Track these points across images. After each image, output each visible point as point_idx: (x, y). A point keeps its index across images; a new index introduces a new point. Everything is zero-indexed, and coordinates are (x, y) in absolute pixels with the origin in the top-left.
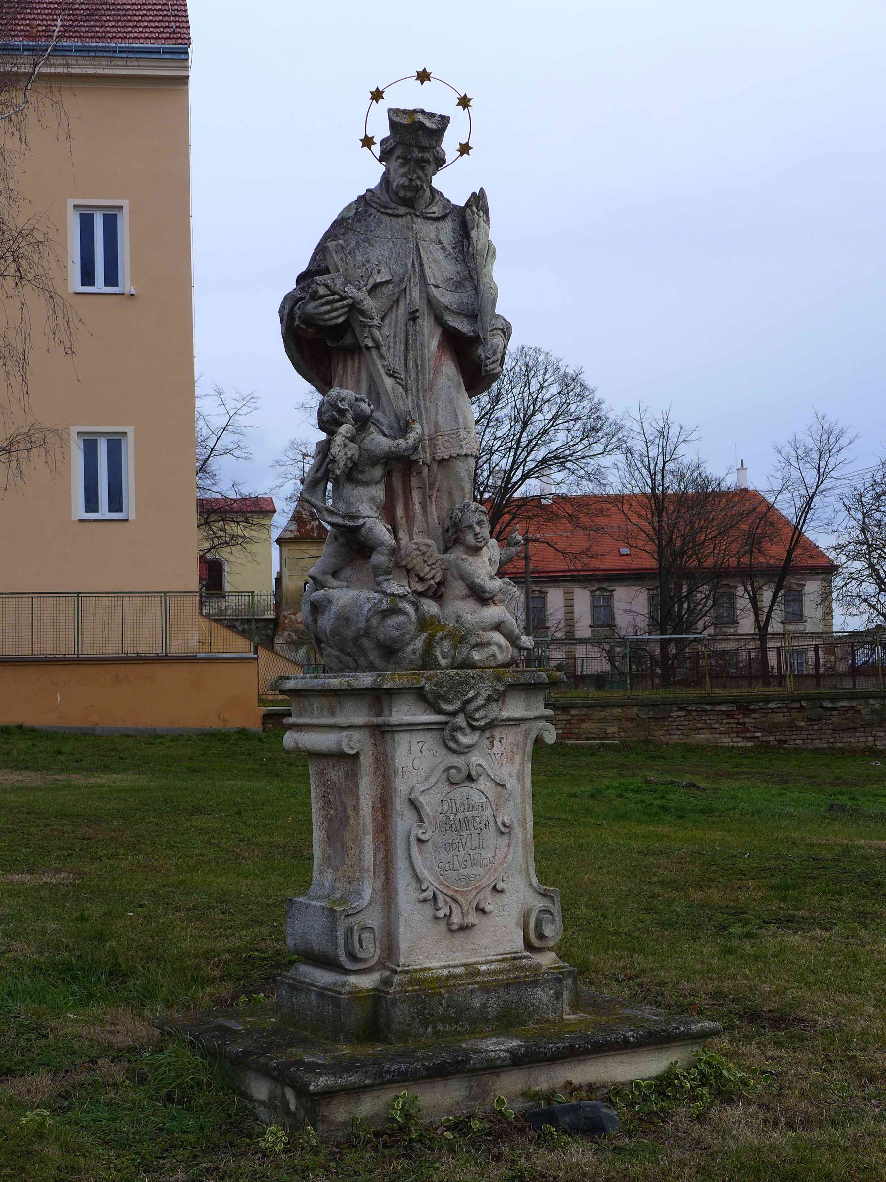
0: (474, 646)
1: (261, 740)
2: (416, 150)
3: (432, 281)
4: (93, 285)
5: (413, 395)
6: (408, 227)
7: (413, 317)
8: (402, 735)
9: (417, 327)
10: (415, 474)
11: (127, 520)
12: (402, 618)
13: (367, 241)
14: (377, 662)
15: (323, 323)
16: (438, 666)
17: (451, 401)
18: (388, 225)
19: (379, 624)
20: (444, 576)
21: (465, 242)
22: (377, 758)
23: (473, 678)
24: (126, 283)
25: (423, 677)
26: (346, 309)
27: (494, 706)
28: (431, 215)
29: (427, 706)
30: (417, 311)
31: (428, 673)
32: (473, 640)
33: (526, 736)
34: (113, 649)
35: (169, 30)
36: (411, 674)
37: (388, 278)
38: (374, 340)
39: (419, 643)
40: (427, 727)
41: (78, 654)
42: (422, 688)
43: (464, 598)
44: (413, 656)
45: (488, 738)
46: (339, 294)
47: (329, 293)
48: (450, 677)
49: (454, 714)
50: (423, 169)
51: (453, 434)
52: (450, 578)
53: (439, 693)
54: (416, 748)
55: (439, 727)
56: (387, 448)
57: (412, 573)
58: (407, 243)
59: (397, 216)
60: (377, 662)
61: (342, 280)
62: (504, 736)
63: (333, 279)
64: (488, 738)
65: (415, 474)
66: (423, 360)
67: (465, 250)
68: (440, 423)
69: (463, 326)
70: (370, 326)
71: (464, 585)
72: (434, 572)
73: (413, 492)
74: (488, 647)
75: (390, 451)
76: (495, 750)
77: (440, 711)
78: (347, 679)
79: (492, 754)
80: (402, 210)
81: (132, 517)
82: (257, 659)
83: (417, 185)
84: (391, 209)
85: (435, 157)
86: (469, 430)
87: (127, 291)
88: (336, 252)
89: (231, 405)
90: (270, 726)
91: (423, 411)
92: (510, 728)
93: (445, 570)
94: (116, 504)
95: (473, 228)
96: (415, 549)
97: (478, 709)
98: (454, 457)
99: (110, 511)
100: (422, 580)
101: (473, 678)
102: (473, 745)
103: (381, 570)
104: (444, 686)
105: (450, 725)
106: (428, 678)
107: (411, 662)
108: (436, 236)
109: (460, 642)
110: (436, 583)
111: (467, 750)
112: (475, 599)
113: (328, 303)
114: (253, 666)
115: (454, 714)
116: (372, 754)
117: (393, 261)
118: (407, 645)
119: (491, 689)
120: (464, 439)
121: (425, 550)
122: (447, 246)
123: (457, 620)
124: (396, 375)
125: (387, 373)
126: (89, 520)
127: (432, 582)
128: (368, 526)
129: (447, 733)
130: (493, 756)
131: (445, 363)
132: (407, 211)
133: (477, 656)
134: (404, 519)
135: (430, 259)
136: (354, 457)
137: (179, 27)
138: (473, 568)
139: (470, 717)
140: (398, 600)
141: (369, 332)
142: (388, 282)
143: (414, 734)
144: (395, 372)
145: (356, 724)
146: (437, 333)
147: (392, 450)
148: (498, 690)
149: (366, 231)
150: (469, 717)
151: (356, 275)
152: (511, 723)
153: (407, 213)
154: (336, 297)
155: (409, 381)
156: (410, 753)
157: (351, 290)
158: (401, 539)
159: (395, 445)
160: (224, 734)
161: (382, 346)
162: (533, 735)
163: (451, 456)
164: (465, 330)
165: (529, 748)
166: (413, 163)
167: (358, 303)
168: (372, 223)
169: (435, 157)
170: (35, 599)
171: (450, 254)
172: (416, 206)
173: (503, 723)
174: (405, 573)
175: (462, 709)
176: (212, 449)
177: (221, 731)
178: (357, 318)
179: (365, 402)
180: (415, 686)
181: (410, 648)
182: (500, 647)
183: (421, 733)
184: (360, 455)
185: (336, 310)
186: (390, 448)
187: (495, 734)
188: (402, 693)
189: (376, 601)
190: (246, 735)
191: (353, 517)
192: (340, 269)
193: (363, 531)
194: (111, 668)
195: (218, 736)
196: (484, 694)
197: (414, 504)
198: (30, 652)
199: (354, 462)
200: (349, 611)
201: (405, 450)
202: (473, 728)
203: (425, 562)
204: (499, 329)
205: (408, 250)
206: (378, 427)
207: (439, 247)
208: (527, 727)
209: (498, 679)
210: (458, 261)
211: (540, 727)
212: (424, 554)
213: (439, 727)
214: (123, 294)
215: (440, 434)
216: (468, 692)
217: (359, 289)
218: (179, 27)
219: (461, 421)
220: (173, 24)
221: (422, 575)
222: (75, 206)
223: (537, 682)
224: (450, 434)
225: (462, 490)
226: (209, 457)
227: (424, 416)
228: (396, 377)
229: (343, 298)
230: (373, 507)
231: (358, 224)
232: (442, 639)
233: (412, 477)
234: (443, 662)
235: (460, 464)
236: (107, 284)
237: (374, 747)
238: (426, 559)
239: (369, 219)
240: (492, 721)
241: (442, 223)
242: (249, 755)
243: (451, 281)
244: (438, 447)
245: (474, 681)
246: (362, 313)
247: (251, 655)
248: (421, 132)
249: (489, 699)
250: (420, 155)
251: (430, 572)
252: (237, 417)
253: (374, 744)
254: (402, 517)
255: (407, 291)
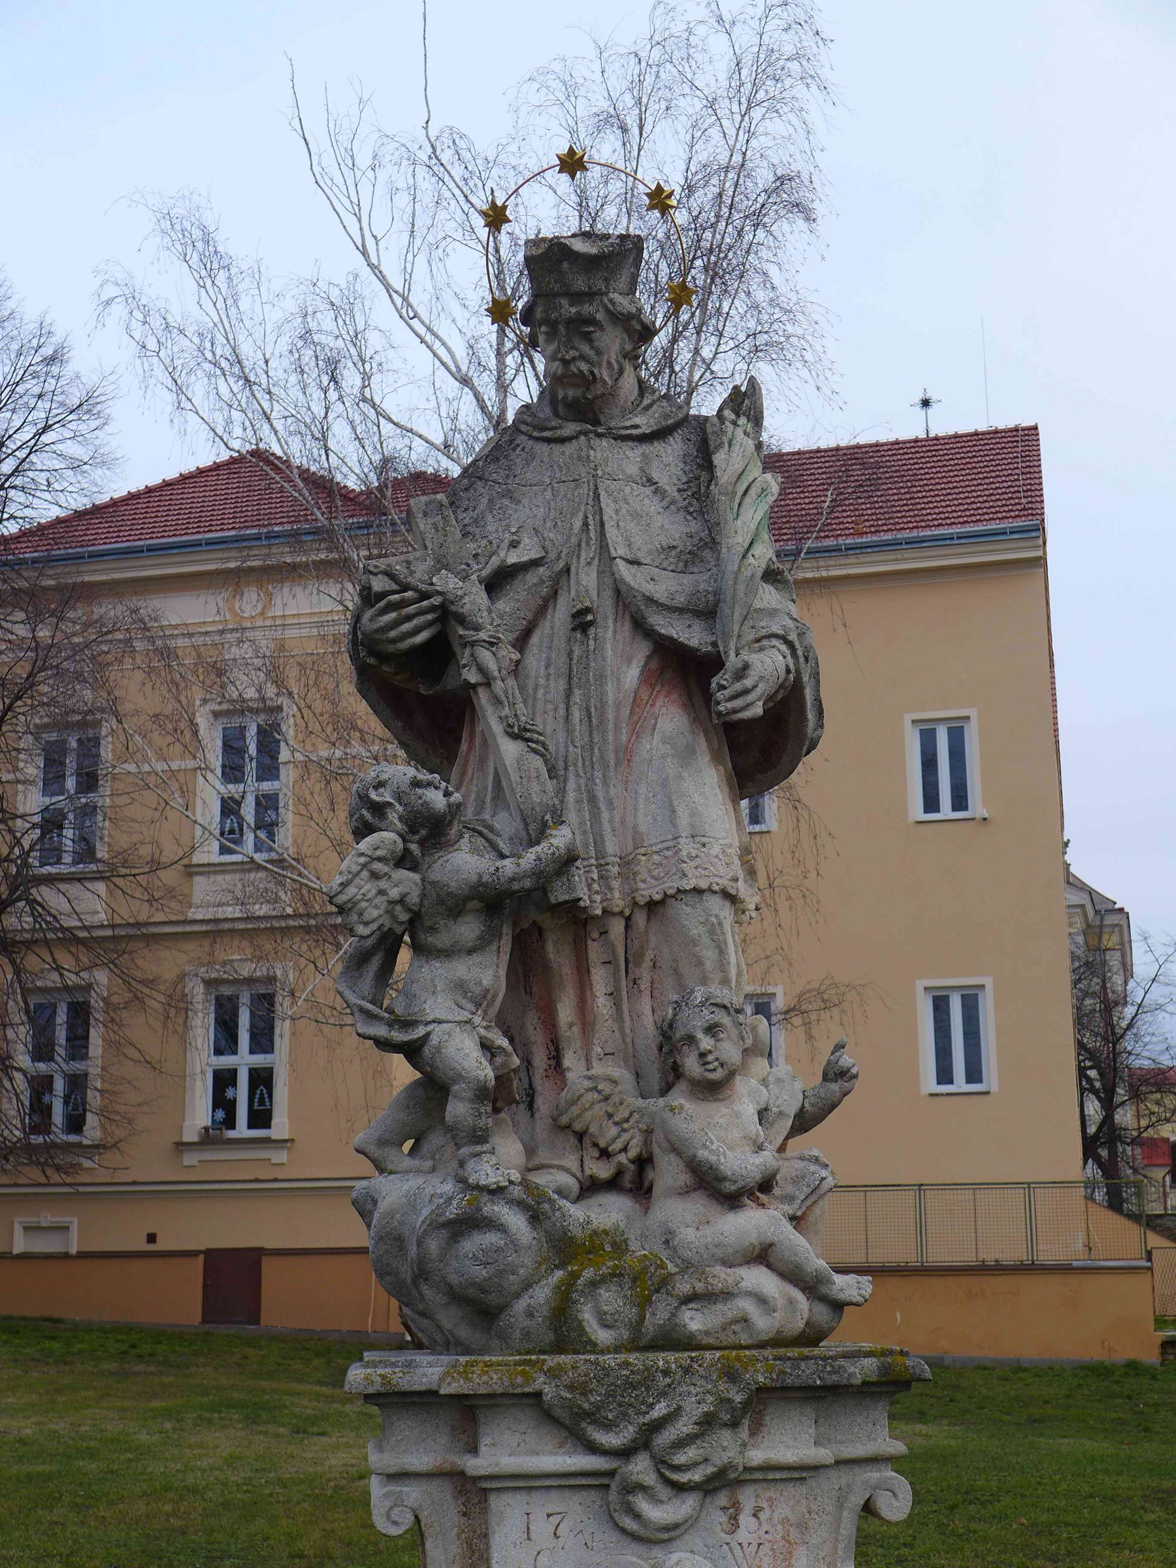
0: (687, 1300)
1: (1154, 1377)
2: (565, 302)
3: (621, 551)
4: (938, 811)
5: (578, 776)
6: (580, 458)
7: (582, 622)
8: (507, 1498)
9: (591, 642)
10: (595, 935)
11: (987, 1093)
12: (490, 1238)
13: (508, 494)
14: (464, 1333)
15: (391, 648)
16: (591, 1346)
17: (664, 784)
18: (546, 459)
19: (445, 1251)
20: (647, 1143)
21: (704, 476)
22: (470, 1546)
23: (666, 1373)
24: (977, 806)
25: (541, 1370)
26: (429, 617)
27: (726, 1436)
28: (628, 432)
29: (564, 1433)
30: (588, 610)
31: (551, 1361)
32: (683, 1287)
33: (840, 1504)
34: (966, 1257)
35: (1019, 507)
36: (517, 1364)
37: (535, 554)
38: (481, 670)
39: (542, 1294)
40: (566, 1482)
41: (922, 1262)
42: (538, 1395)
43: (685, 1192)
44: (528, 1322)
45: (724, 1509)
46: (415, 589)
47: (395, 587)
48: (607, 1371)
49: (626, 1453)
50: (588, 337)
51: (668, 849)
52: (657, 1151)
53: (580, 1407)
54: (542, 1528)
55: (598, 1482)
56: (474, 878)
57: (587, 1141)
58: (577, 487)
59: (562, 440)
60: (464, 1333)
61: (430, 562)
62: (765, 1505)
63: (408, 563)
64: (724, 1509)
65: (595, 935)
66: (603, 705)
67: (703, 490)
68: (643, 828)
69: (692, 635)
70: (473, 644)
71: (682, 1165)
72: (626, 1136)
73: (593, 971)
74: (725, 1300)
75: (480, 883)
76: (742, 1535)
77: (593, 1448)
78: (380, 1371)
79: (734, 1544)
80: (570, 428)
81: (994, 1088)
82: (1150, 1269)
83: (582, 371)
84: (551, 429)
85: (608, 311)
86: (704, 840)
87: (977, 816)
88: (425, 514)
89: (1160, 950)
90: (1172, 1357)
91: (603, 808)
92: (780, 1486)
93: (648, 1132)
94: (974, 1074)
95: (721, 445)
96: (588, 1090)
97: (681, 1444)
98: (673, 896)
99: (939, 1083)
100: (605, 1154)
101: (666, 1373)
102: (676, 1526)
103: (462, 1134)
104: (591, 1391)
105: (617, 1478)
106: (554, 1373)
107: (527, 1335)
108: (641, 469)
109: (658, 1291)
110: (632, 1162)
111: (666, 1536)
112: (709, 1196)
113: (391, 607)
114: (1145, 1278)
115: (626, 1453)
116: (459, 1536)
117: (549, 524)
118: (518, 1296)
119: (710, 1399)
120: (692, 858)
121: (607, 1091)
122: (667, 487)
123: (667, 1242)
124: (528, 735)
125: (508, 733)
126: (942, 1095)
127: (622, 1158)
128: (434, 1040)
129: (613, 1495)
130: (738, 1550)
131: (664, 710)
132: (578, 428)
133: (694, 1321)
134: (575, 1029)
135: (624, 512)
136: (408, 899)
137: (1031, 502)
138: (694, 1127)
139: (663, 1462)
140: (485, 1198)
141: (472, 655)
142: (535, 563)
143: (536, 1497)
144: (526, 730)
145: (412, 1469)
146: (642, 650)
147: (484, 879)
148: (729, 1401)
149: (508, 477)
150: (661, 1463)
151: (464, 554)
152: (778, 1476)
153: (580, 433)
154: (409, 594)
155: (571, 749)
156: (529, 1539)
157: (447, 582)
158: (568, 1069)
159: (492, 870)
160: (1106, 1368)
161: (495, 678)
162: (857, 1500)
163: (665, 894)
164: (694, 642)
165: (848, 1526)
166: (562, 329)
167: (452, 603)
168: (518, 461)
169: (608, 311)
170: (978, 1192)
171: (673, 502)
172: (602, 418)
173: (758, 1475)
174: (573, 1140)
175: (643, 1442)
176: (1140, 1006)
177: (1102, 1363)
178: (456, 632)
179: (437, 788)
180: (519, 1391)
181: (520, 1306)
182: (762, 1300)
183: (554, 1494)
184: (423, 896)
185: (409, 618)
186: (480, 876)
187: (741, 1498)
188: (498, 1406)
189: (441, 1201)
190: (1136, 1369)
191: (407, 1024)
192: (428, 544)
193: (426, 1051)
194: (963, 1279)
195: (1098, 1371)
196: (694, 1410)
197: (594, 997)
198: (864, 1260)
199: (409, 910)
200: (401, 1223)
201: (512, 880)
202: (680, 1488)
203: (610, 1116)
204: (776, 636)
205: (577, 500)
206: (487, 840)
207: (648, 491)
208: (844, 1481)
209: (731, 1375)
210: (690, 514)
211: (873, 1482)
212: (606, 1099)
213: (598, 1482)
214: (973, 819)
215: (643, 850)
216: (651, 1406)
217: (465, 578)
218: (1031, 502)
219: (683, 820)
220: (1024, 501)
221: (602, 1144)
222: (913, 722)
223: (829, 1382)
224: (661, 850)
225: (699, 963)
226: (1136, 1015)
227: (605, 816)
228: (528, 740)
229: (424, 596)
230: (464, 1002)
231: (492, 467)
232: (594, 1284)
233: (589, 942)
234: (603, 1336)
235: (688, 910)
236: (954, 809)
237: (463, 1520)
238: (610, 1110)
239: (513, 455)
240: (722, 1472)
241: (658, 447)
242: (1129, 1397)
243: (673, 553)
244: (639, 877)
245: (668, 1380)
246: (462, 620)
247: (1144, 1263)
248: (565, 265)
249: (708, 1423)
250: (573, 310)
251: (619, 1136)
252: (1168, 965)
253: (464, 1514)
254: (571, 1025)
255: (572, 575)
